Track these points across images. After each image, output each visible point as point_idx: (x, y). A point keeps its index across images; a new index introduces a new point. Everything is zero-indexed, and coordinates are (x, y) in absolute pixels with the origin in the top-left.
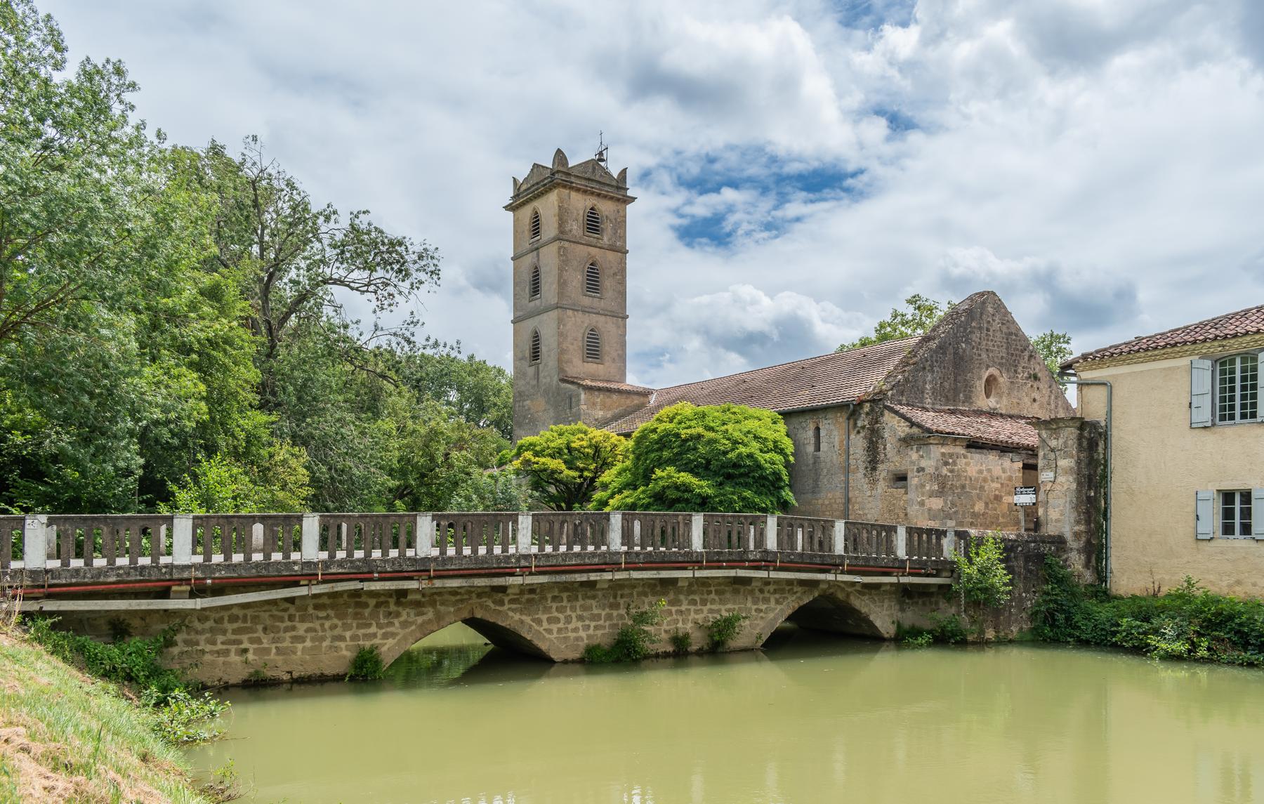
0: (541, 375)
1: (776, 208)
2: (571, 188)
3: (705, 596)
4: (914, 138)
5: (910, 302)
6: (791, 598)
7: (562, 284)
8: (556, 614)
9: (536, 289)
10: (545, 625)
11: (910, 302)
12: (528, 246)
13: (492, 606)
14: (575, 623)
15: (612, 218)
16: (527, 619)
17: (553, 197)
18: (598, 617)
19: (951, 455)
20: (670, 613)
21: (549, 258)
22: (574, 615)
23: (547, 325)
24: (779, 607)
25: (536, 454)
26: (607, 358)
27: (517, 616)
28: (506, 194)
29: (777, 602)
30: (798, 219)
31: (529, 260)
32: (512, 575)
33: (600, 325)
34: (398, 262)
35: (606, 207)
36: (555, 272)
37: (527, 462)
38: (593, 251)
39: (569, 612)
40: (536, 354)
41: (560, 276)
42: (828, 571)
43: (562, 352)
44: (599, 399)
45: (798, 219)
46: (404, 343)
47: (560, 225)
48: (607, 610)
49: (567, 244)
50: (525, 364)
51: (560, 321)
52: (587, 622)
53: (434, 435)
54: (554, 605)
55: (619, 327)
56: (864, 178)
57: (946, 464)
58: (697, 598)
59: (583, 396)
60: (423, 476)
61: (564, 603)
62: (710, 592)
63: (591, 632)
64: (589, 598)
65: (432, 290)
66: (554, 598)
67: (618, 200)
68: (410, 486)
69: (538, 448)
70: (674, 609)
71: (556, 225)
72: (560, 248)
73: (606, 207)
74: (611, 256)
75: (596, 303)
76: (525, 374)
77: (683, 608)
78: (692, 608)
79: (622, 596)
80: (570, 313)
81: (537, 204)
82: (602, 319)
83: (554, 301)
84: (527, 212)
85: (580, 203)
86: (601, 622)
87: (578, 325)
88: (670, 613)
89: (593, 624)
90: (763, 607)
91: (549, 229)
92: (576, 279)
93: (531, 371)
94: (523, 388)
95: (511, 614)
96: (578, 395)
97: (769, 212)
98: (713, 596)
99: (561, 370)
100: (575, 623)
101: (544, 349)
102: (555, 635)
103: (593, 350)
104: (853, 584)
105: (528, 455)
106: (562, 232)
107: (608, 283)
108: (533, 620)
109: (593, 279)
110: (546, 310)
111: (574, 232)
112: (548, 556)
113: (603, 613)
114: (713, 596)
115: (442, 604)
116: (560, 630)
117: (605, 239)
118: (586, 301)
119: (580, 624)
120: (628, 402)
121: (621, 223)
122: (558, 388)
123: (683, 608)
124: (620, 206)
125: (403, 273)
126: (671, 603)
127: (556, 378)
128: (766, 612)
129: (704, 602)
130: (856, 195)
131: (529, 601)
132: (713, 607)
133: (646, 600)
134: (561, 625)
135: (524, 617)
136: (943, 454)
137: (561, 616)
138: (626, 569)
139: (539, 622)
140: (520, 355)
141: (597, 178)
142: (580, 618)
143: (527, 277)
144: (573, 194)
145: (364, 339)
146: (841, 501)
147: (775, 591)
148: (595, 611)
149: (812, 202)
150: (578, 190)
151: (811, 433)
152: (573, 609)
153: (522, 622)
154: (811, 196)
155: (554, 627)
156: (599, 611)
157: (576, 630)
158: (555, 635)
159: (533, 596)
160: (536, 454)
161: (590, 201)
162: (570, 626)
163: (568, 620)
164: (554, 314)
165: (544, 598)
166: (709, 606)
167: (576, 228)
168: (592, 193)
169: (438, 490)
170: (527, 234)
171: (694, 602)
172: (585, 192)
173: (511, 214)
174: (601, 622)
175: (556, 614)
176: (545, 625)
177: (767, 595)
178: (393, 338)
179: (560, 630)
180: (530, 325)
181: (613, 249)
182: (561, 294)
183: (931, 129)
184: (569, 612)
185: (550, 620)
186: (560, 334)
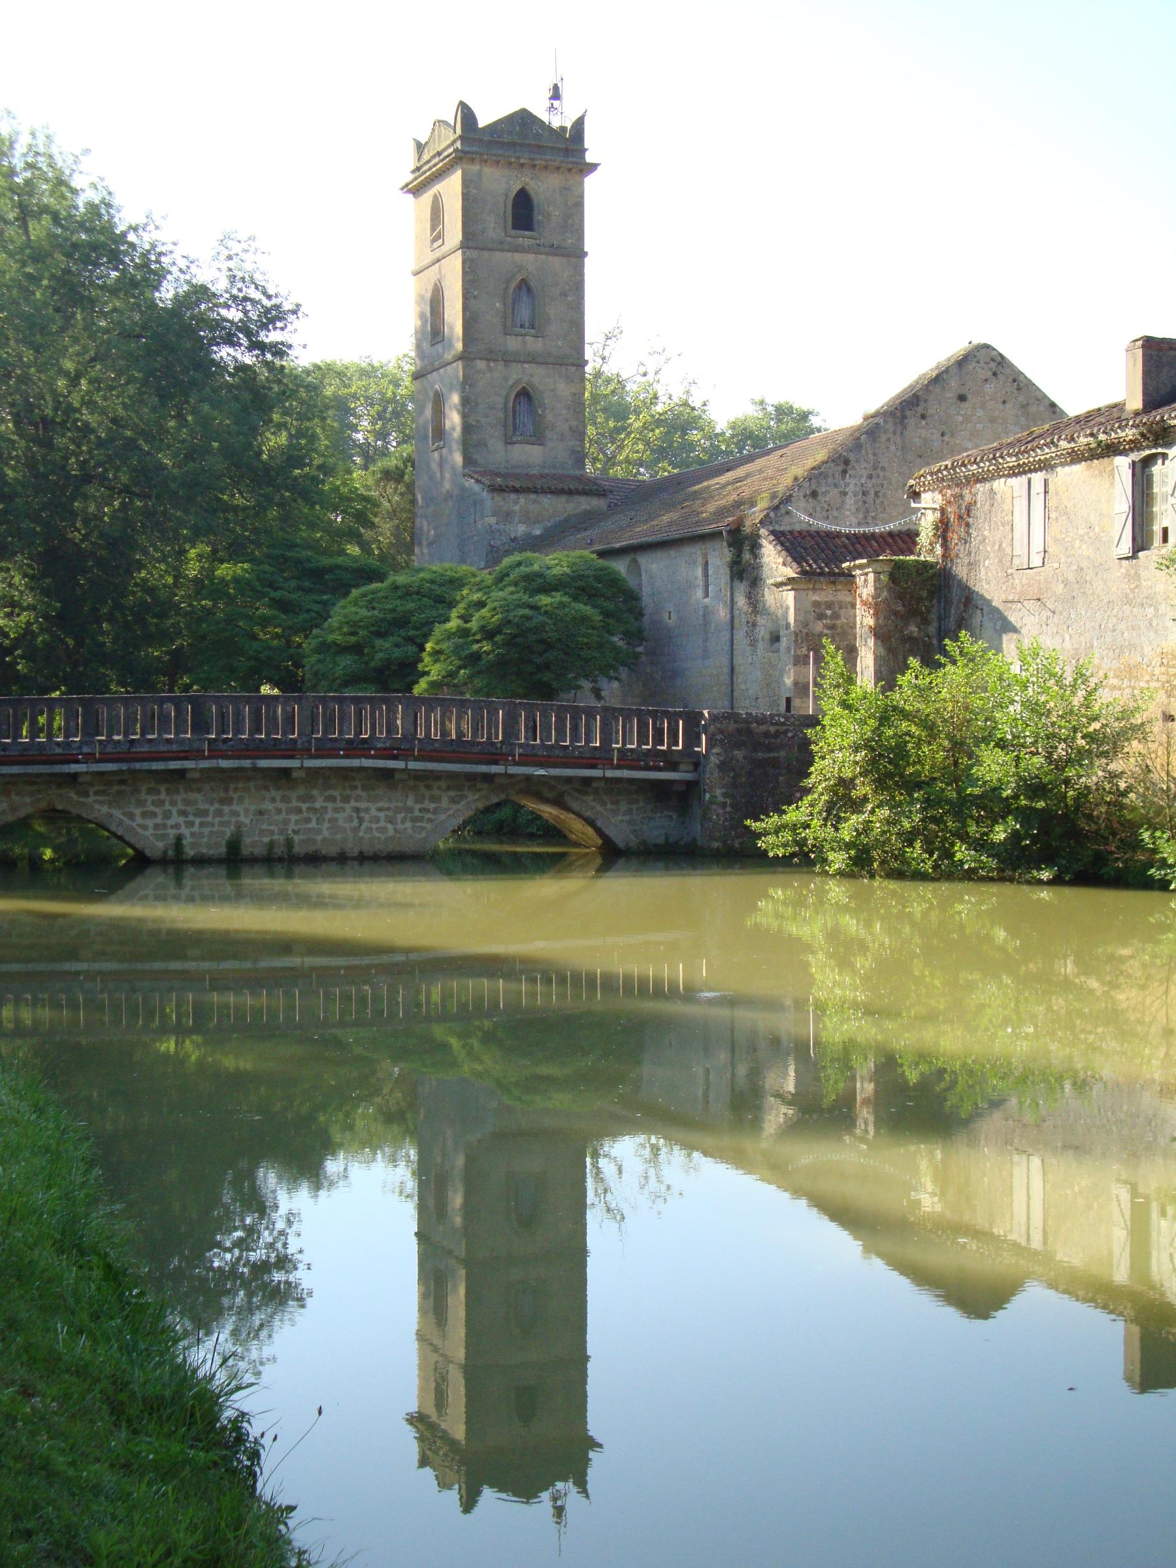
3: (348, 792)
6: (472, 796)
8: (151, 808)
10: (139, 820)
13: (75, 797)
14: (176, 819)
16: (117, 813)
18: (205, 813)
19: (829, 605)
20: (300, 811)
22: (174, 811)
24: (455, 807)
26: (548, 434)
27: (105, 809)
28: (404, 168)
29: (453, 801)
31: (432, 274)
32: (77, 762)
33: (536, 380)
35: (544, 187)
39: (167, 807)
42: (496, 763)
48: (217, 806)
52: (191, 818)
54: (150, 798)
57: (821, 617)
58: (336, 793)
61: (163, 796)
62: (356, 788)
63: (196, 829)
64: (192, 790)
66: (150, 791)
70: (304, 806)
74: (556, 262)
75: (534, 345)
77: (317, 805)
78: (330, 805)
79: (236, 790)
81: (438, 188)
84: (427, 197)
86: (209, 819)
88: (300, 811)
89: (198, 821)
90: (432, 806)
95: (97, 806)
98: (359, 792)
100: (176, 819)
102: (151, 831)
104: (569, 780)
108: (125, 814)
112: (168, 741)
113: (212, 809)
114: (359, 792)
115: (18, 794)
116: (156, 826)
119: (181, 820)
123: (317, 805)
126: (301, 799)
128: (435, 812)
129: (346, 799)
131: (119, 793)
132: (358, 805)
133: (268, 795)
134: (159, 820)
135: (113, 811)
136: (816, 604)
137: (157, 810)
138: (210, 757)
139: (131, 816)
142: (183, 813)
146: (726, 670)
147: (449, 788)
148: (202, 806)
151: (699, 572)
152: (174, 803)
153: (111, 815)
155: (150, 823)
156: (207, 806)
157: (177, 826)
158: (151, 831)
159: (124, 787)
162: (170, 822)
163: (167, 815)
165: (137, 791)
166: (353, 803)
171: (332, 799)
174: (209, 819)
175: (151, 808)
176: (139, 820)
177: (436, 792)
179: (156, 826)
181: (555, 250)
184: (167, 807)
185: (144, 815)
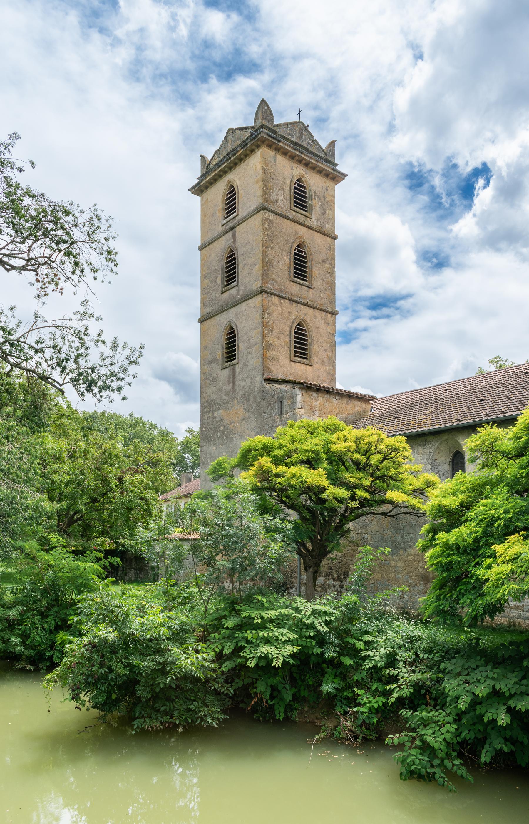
0: (238, 377)
1: (352, 321)
2: (278, 149)
4: (447, 273)
5: (491, 362)
7: (267, 265)
9: (230, 275)
11: (491, 362)
12: (220, 229)
15: (321, 195)
17: (255, 162)
21: (249, 236)
23: (246, 319)
25: (277, 461)
26: (315, 359)
30: (365, 330)
31: (222, 245)
33: (308, 319)
34: (66, 242)
35: (314, 182)
36: (258, 251)
37: (265, 475)
38: (302, 230)
40: (231, 353)
41: (264, 254)
43: (267, 346)
44: (318, 400)
45: (365, 330)
46: (70, 337)
47: (265, 193)
49: (272, 217)
50: (217, 368)
51: (264, 309)
53: (109, 458)
55: (328, 324)
56: (410, 300)
59: (299, 398)
60: (94, 500)
65: (107, 279)
67: (327, 175)
68: (80, 511)
69: (278, 452)
71: (260, 193)
72: (264, 220)
73: (314, 182)
74: (319, 238)
76: (215, 380)
80: (275, 299)
82: (311, 311)
83: (256, 285)
84: (218, 191)
85: (288, 171)
87: (284, 317)
91: (247, 203)
92: (284, 262)
93: (224, 375)
94: (213, 397)
96: (293, 397)
97: (347, 324)
99: (266, 368)
101: (241, 346)
103: (301, 345)
105: (265, 462)
106: (267, 201)
107: (316, 270)
109: (300, 267)
110: (246, 298)
111: (280, 203)
117: (314, 219)
118: (294, 289)
120: (349, 408)
121: (329, 204)
122: (263, 391)
124: (329, 183)
125: (69, 248)
127: (259, 380)
130: (406, 314)
140: (209, 358)
141: (305, 144)
143: (219, 265)
144: (279, 158)
145: (20, 331)
149: (376, 318)
150: (285, 153)
154: (374, 313)
160: (277, 461)
161: (298, 171)
164: (257, 301)
167: (283, 199)
168: (300, 161)
169: (109, 516)
170: (220, 214)
172: (292, 157)
173: (197, 199)
178: (58, 333)
180: (223, 319)
182: (265, 276)
183: (460, 267)
186: (265, 325)
